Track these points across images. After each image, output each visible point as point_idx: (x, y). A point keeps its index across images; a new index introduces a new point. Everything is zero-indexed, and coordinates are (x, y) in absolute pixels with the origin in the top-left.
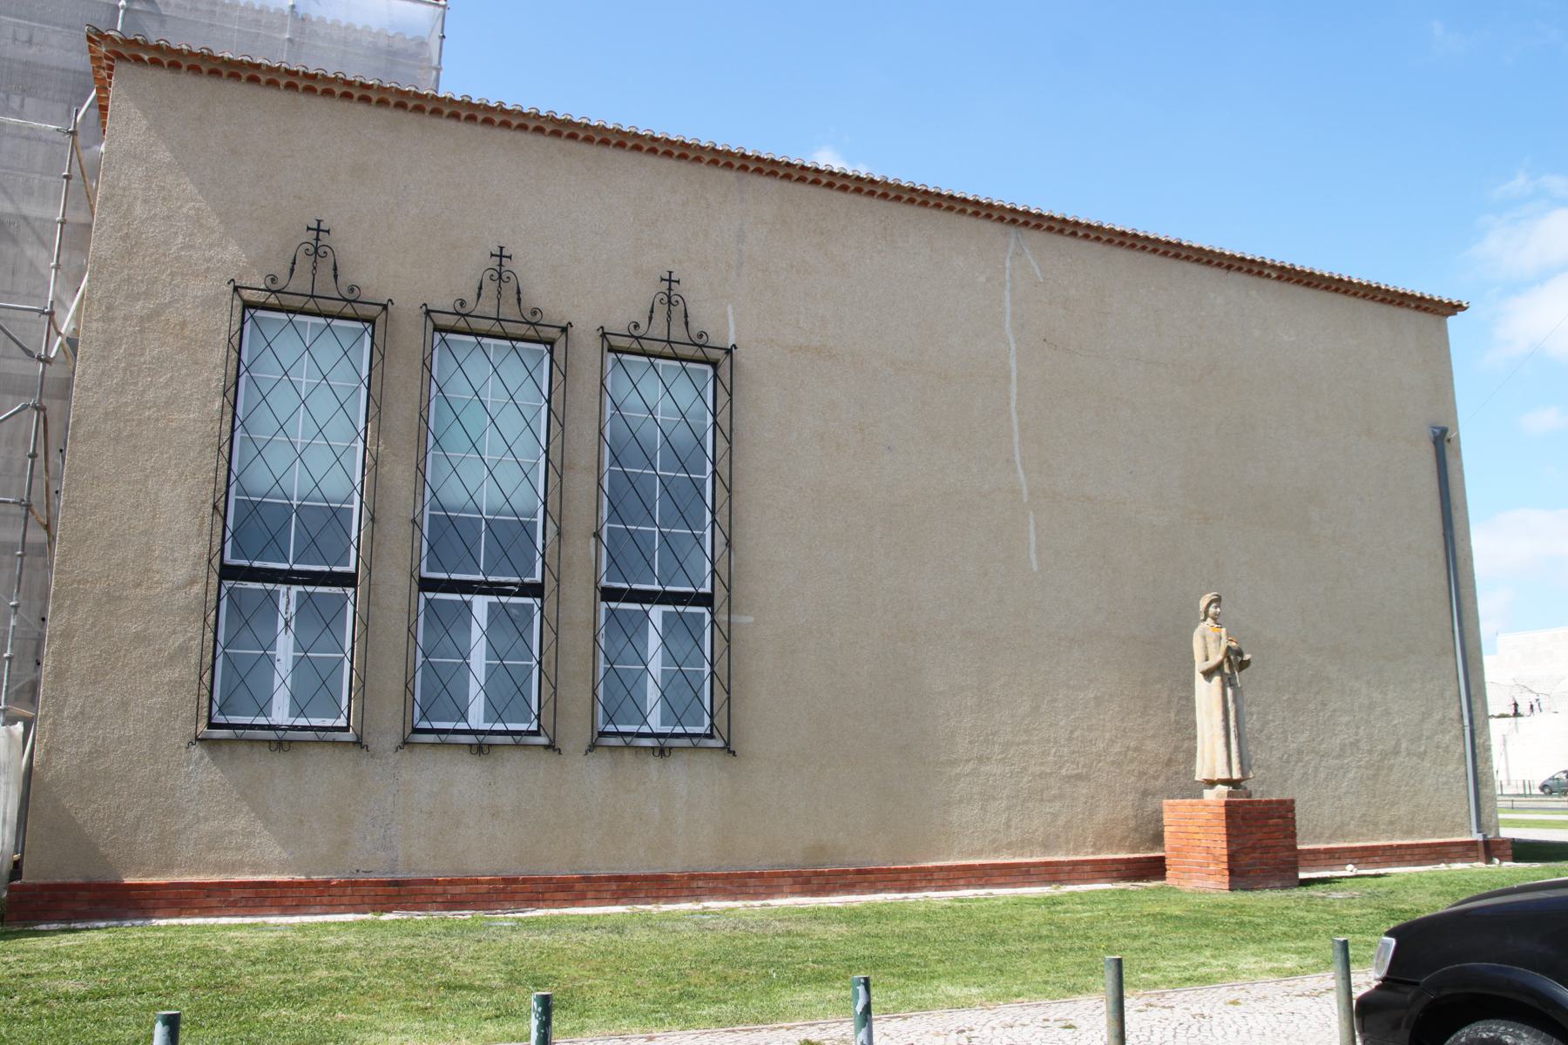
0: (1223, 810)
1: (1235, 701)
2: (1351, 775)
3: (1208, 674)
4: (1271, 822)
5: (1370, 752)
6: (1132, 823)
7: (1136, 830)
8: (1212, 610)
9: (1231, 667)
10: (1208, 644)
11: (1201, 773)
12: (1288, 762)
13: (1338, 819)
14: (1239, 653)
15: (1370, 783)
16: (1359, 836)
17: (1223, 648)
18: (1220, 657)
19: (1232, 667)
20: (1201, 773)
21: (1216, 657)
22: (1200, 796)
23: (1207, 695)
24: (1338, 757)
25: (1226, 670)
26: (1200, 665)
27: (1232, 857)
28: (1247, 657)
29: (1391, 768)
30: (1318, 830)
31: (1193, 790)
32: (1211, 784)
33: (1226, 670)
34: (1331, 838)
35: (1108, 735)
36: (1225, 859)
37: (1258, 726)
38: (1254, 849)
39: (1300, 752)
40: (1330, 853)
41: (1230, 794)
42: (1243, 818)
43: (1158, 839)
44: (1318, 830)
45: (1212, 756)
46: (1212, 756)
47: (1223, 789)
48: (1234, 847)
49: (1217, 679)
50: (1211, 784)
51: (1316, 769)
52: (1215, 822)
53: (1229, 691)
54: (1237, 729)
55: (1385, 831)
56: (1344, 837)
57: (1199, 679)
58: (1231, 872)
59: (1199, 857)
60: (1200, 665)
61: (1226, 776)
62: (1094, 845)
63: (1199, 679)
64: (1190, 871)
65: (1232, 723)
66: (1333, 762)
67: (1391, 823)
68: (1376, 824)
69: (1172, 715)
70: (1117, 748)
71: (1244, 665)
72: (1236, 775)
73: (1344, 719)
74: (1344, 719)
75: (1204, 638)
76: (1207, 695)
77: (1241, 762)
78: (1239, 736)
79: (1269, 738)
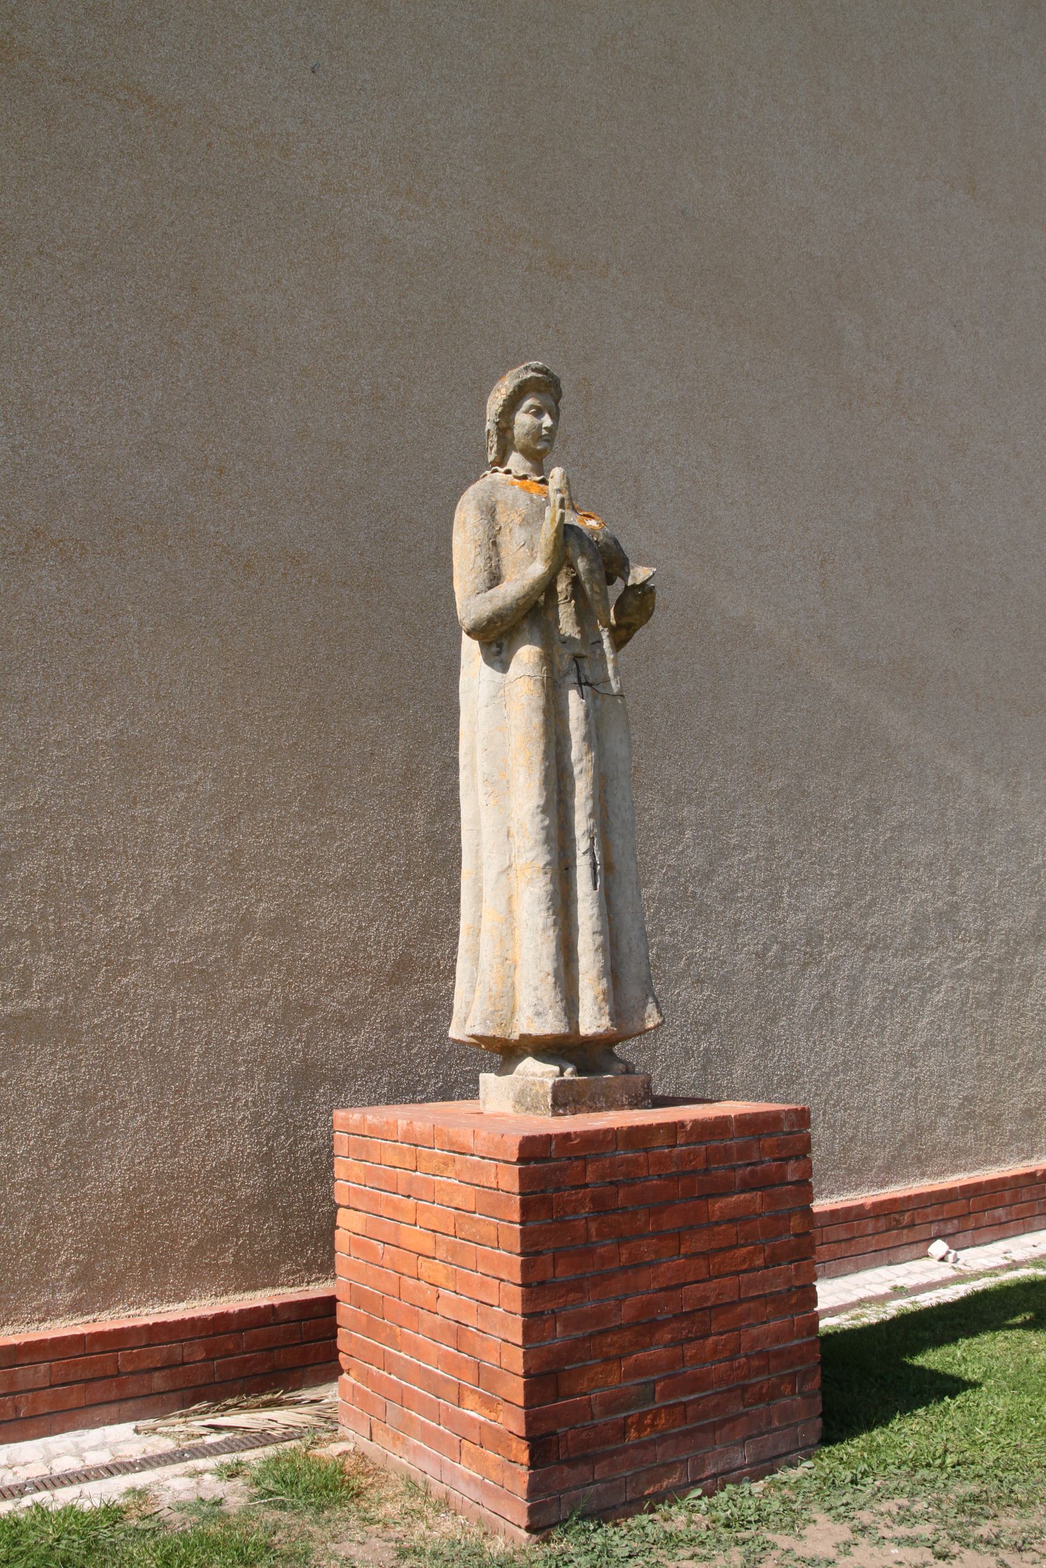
0: (510, 1179)
1: (595, 738)
2: (938, 998)
3: (498, 637)
4: (719, 1206)
5: (982, 936)
6: (249, 1185)
7: (264, 1206)
8: (523, 420)
9: (584, 615)
10: (498, 535)
11: (469, 1019)
12: (780, 964)
13: (907, 1115)
14: (611, 561)
15: (982, 1014)
16: (957, 1157)
17: (547, 531)
18: (538, 569)
19: (588, 609)
20: (469, 1019)
21: (526, 570)
22: (472, 1092)
23: (497, 708)
24: (911, 949)
25: (567, 625)
26: (471, 602)
27: (544, 1382)
28: (640, 574)
29: (1027, 977)
30: (857, 1152)
31: (455, 1071)
32: (506, 1052)
33: (567, 625)
34: (889, 1173)
35: (163, 877)
36: (515, 1388)
37: (697, 860)
38: (645, 1327)
39: (813, 938)
40: (889, 1213)
41: (564, 1099)
42: (601, 1207)
43: (317, 1248)
44: (857, 1152)
45: (506, 953)
46: (506, 953)
47: (538, 1074)
48: (560, 1336)
49: (526, 656)
50: (506, 1052)
51: (855, 983)
52: (486, 1226)
53: (575, 704)
54: (603, 843)
55: (1015, 1136)
56: (921, 1165)
57: (464, 635)
58: (543, 1446)
59: (432, 1356)
60: (471, 602)
61: (550, 1025)
62: (84, 1276)
63: (464, 635)
64: (403, 1399)
65: (582, 823)
66: (899, 964)
67: (1029, 1114)
68: (995, 1121)
69: (420, 818)
70: (198, 923)
71: (638, 605)
72: (592, 1021)
73: (924, 851)
74: (924, 851)
75: (490, 512)
76: (497, 708)
77: (614, 972)
78: (606, 874)
79: (728, 897)
